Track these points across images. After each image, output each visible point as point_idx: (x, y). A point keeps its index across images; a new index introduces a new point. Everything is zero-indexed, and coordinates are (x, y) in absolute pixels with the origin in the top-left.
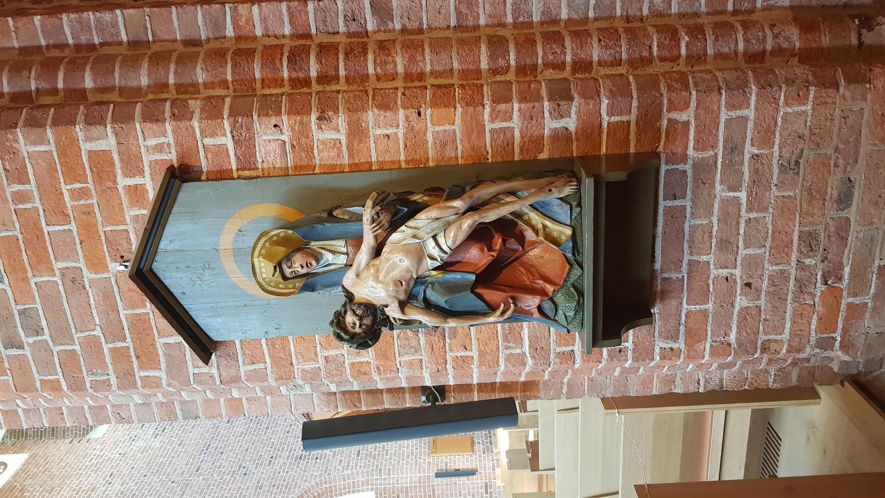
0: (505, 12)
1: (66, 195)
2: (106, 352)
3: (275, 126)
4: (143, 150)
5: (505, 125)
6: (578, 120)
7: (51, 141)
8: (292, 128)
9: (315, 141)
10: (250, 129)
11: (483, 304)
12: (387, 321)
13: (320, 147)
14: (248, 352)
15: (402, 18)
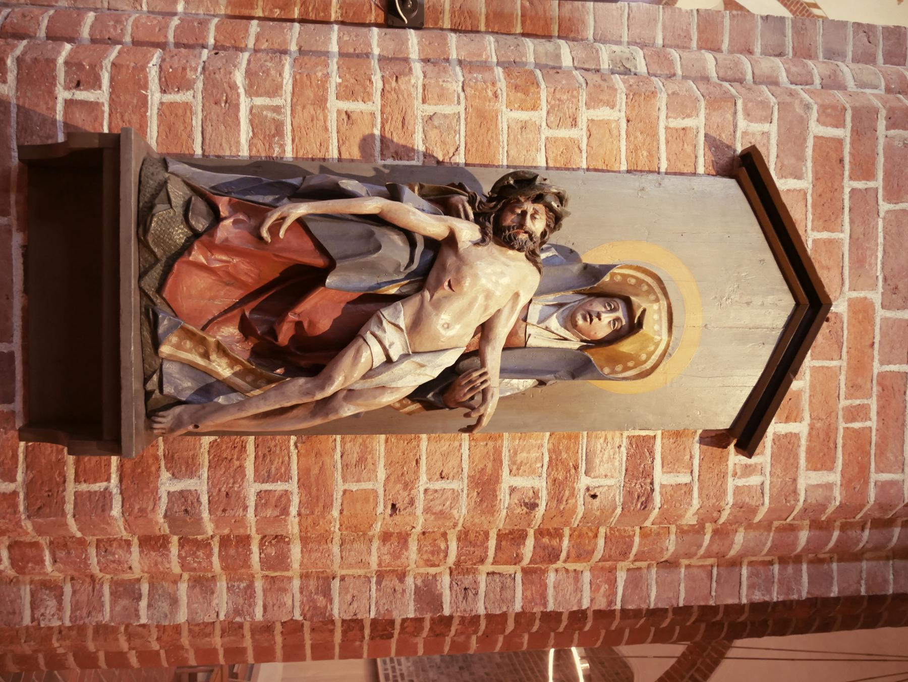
0: (265, 595)
1: (873, 414)
2: (880, 175)
3: (594, 496)
4: (768, 469)
6: (156, 489)
7: (872, 485)
9: (544, 475)
13: (539, 465)
15: (404, 591)
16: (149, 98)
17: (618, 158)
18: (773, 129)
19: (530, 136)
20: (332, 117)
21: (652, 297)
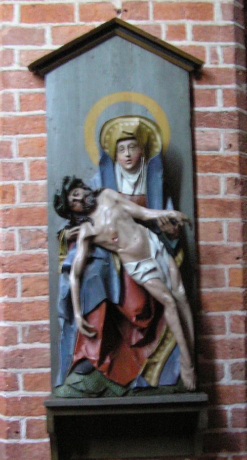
4: (213, 44)
5: (228, 328)
6: (230, 386)
8: (228, 158)
10: (229, 126)
16: (23, 396)
18: (17, 48)
20: (25, 299)
21: (116, 127)
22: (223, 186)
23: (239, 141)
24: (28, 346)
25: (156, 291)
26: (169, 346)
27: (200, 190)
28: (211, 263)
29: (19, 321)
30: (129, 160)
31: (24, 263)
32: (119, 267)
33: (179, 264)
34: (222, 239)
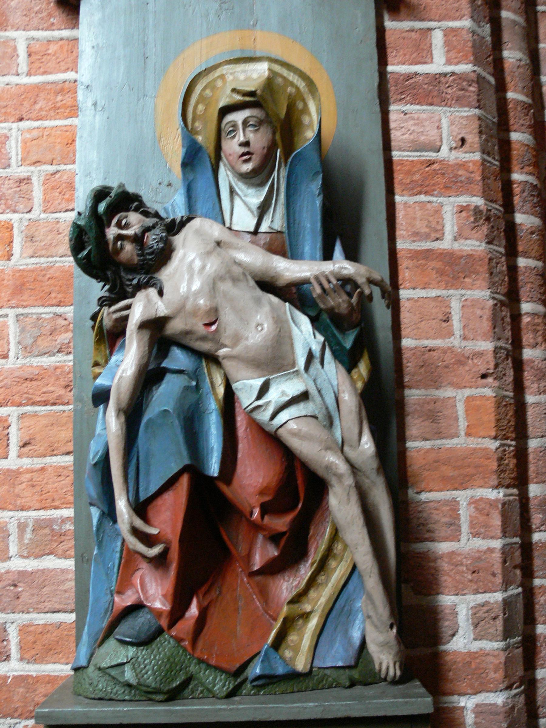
3: (463, 140)
5: (465, 528)
6: (470, 653)
9: (441, 200)
10: (459, 101)
11: (153, 489)
12: (119, 293)
13: (429, 206)
14: (53, 48)
16: (16, 674)
17: (65, 129)
19: (43, 231)
20: (26, 463)
21: (219, 83)
22: (450, 226)
23: (480, 132)
24: (30, 565)
25: (310, 446)
26: (338, 573)
27: (400, 232)
28: (426, 387)
29: (11, 510)
30: (243, 154)
31: (24, 385)
32: (221, 391)
33: (360, 385)
34: (451, 334)
